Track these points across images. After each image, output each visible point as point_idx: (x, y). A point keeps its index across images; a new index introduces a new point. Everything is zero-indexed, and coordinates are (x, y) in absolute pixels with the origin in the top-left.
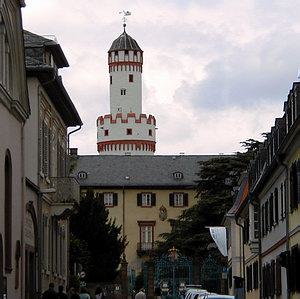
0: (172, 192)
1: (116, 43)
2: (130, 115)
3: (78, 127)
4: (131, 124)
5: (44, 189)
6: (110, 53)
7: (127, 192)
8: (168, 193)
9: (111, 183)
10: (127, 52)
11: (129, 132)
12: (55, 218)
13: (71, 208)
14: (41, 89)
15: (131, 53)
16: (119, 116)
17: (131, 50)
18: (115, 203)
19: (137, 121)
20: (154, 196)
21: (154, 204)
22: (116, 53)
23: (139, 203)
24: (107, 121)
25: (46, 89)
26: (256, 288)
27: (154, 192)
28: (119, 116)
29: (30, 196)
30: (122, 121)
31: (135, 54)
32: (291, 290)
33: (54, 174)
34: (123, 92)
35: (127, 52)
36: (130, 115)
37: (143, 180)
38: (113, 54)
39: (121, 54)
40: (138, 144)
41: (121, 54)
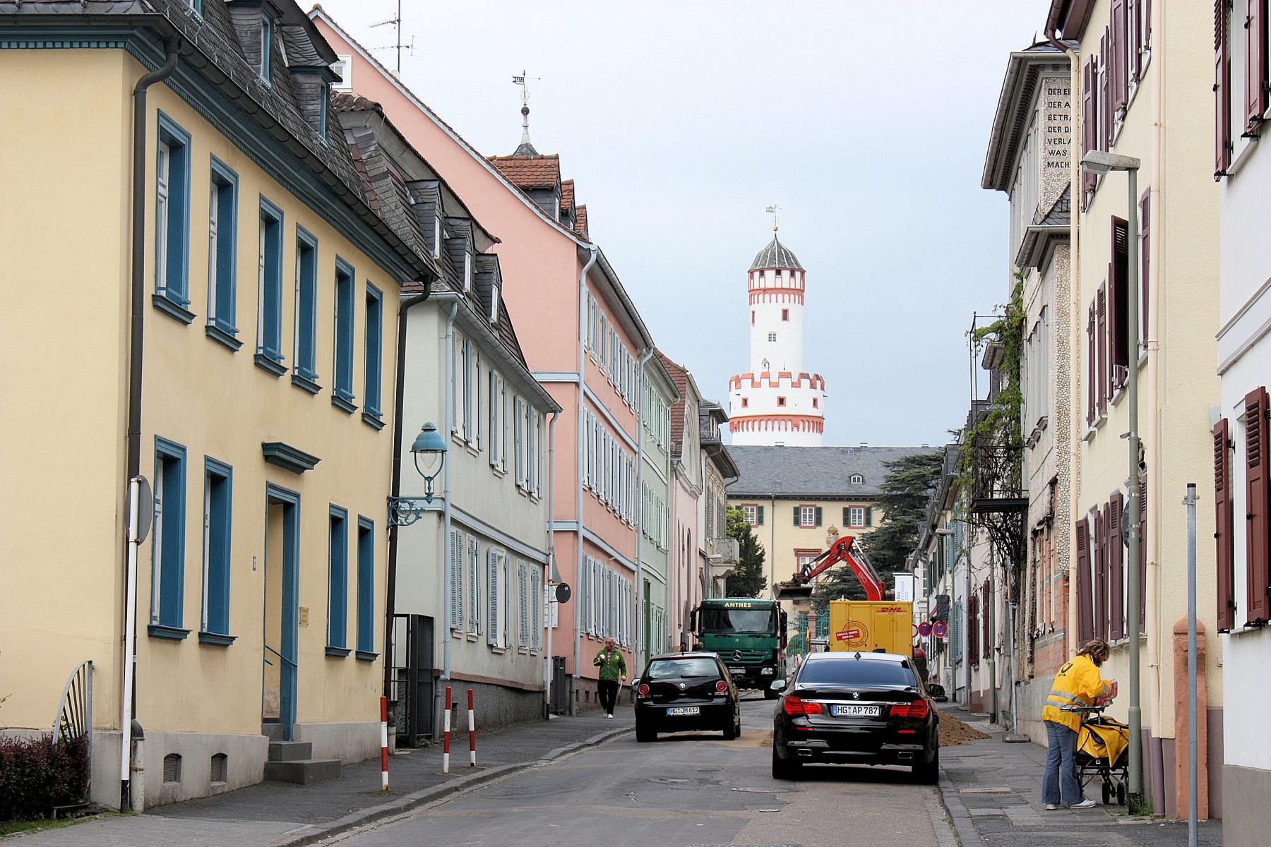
0: (846, 505)
1: (763, 256)
2: (784, 375)
3: (735, 478)
4: (785, 388)
5: (709, 556)
6: (751, 273)
7: (777, 503)
8: (842, 505)
9: (754, 491)
10: (778, 272)
11: (781, 401)
12: (716, 578)
13: (732, 569)
14: (709, 460)
15: (786, 274)
16: (766, 376)
17: (785, 269)
18: (760, 521)
19: (793, 385)
20: (819, 511)
21: (819, 522)
22: (762, 273)
23: (797, 522)
24: (746, 383)
25: (714, 459)
26: (365, 656)
27: (819, 504)
28: (766, 376)
29: (701, 563)
30: (771, 384)
31: (792, 274)
32: (980, 691)
33: (715, 536)
34: (772, 337)
35: (778, 272)
36: (784, 375)
37: (796, 490)
38: (757, 274)
39: (770, 274)
40: (797, 421)
41: (770, 274)
